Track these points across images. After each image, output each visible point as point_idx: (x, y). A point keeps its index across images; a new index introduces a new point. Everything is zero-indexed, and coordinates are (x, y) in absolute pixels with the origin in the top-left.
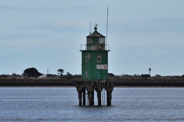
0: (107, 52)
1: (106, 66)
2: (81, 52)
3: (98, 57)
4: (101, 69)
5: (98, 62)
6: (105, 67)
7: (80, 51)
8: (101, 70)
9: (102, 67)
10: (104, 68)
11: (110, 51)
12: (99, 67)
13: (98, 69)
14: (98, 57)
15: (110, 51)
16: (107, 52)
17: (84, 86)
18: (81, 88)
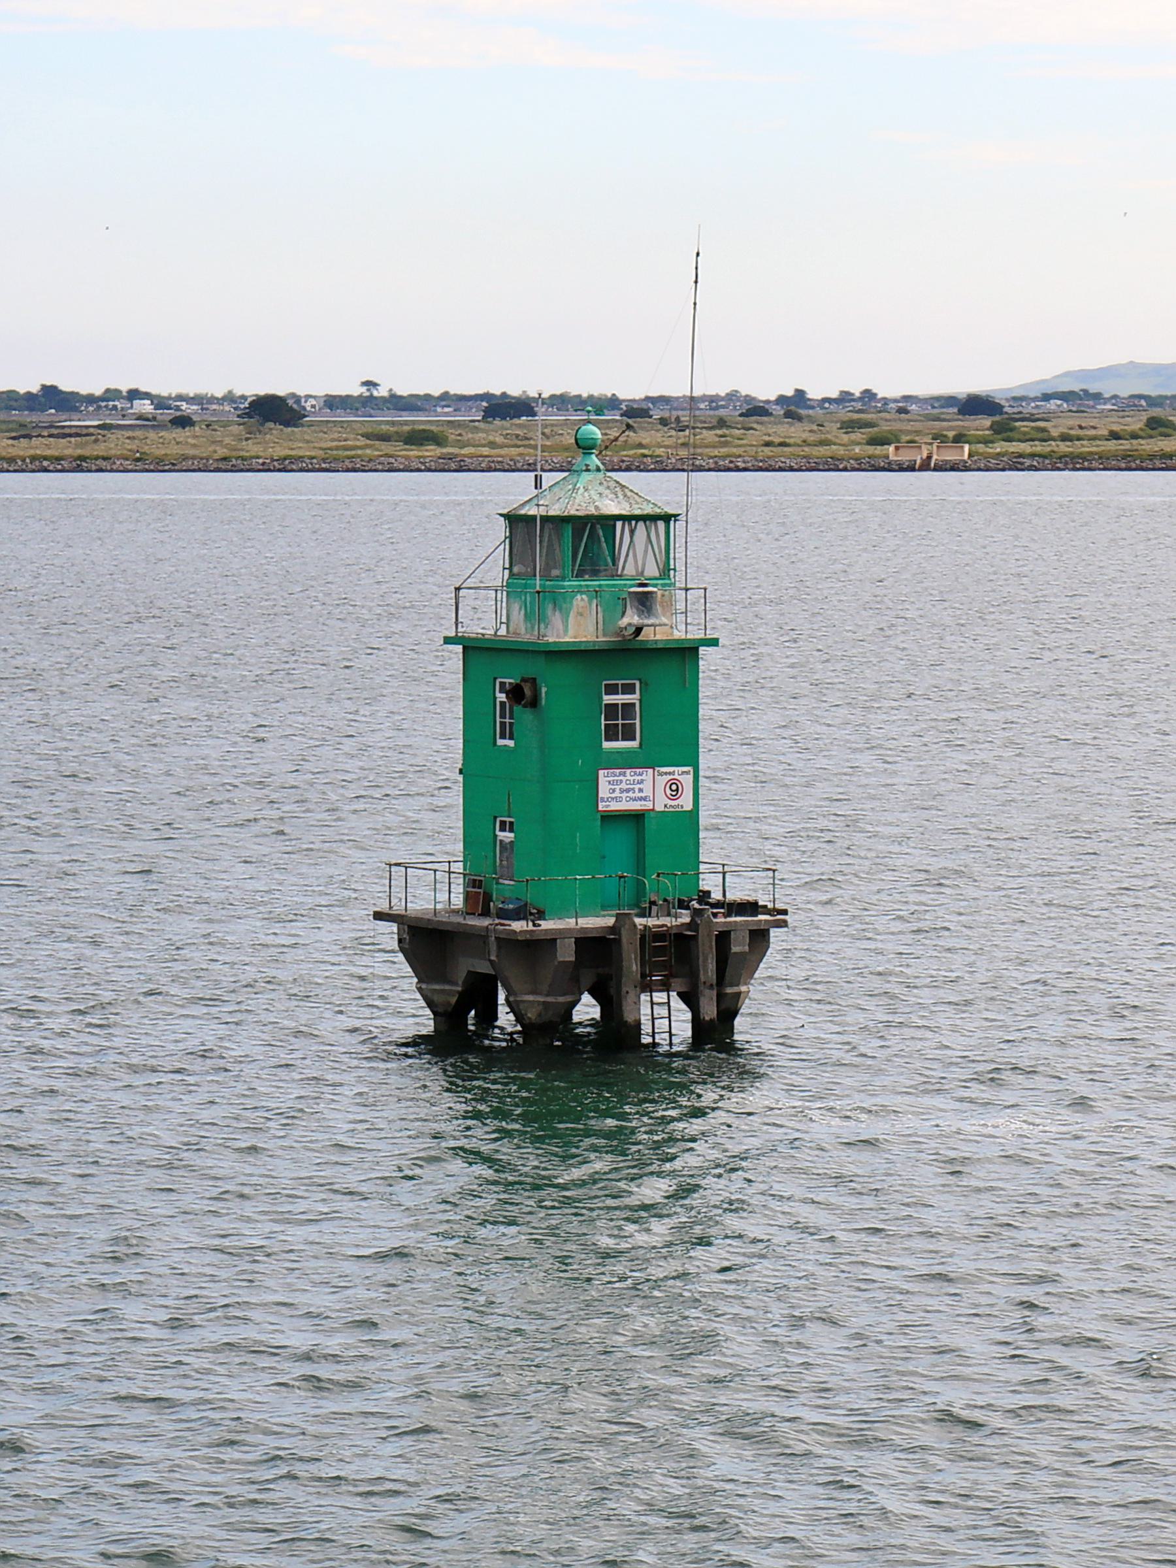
0: (685, 654)
1: (687, 781)
2: (459, 649)
3: (608, 699)
4: (636, 806)
5: (607, 745)
6: (675, 789)
7: (448, 640)
8: (637, 818)
9: (648, 792)
10: (661, 803)
11: (714, 642)
12: (619, 791)
13: (614, 806)
14: (608, 699)
15: (714, 642)
16: (685, 654)
17: (484, 968)
18: (461, 976)
